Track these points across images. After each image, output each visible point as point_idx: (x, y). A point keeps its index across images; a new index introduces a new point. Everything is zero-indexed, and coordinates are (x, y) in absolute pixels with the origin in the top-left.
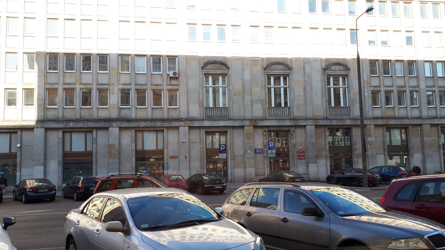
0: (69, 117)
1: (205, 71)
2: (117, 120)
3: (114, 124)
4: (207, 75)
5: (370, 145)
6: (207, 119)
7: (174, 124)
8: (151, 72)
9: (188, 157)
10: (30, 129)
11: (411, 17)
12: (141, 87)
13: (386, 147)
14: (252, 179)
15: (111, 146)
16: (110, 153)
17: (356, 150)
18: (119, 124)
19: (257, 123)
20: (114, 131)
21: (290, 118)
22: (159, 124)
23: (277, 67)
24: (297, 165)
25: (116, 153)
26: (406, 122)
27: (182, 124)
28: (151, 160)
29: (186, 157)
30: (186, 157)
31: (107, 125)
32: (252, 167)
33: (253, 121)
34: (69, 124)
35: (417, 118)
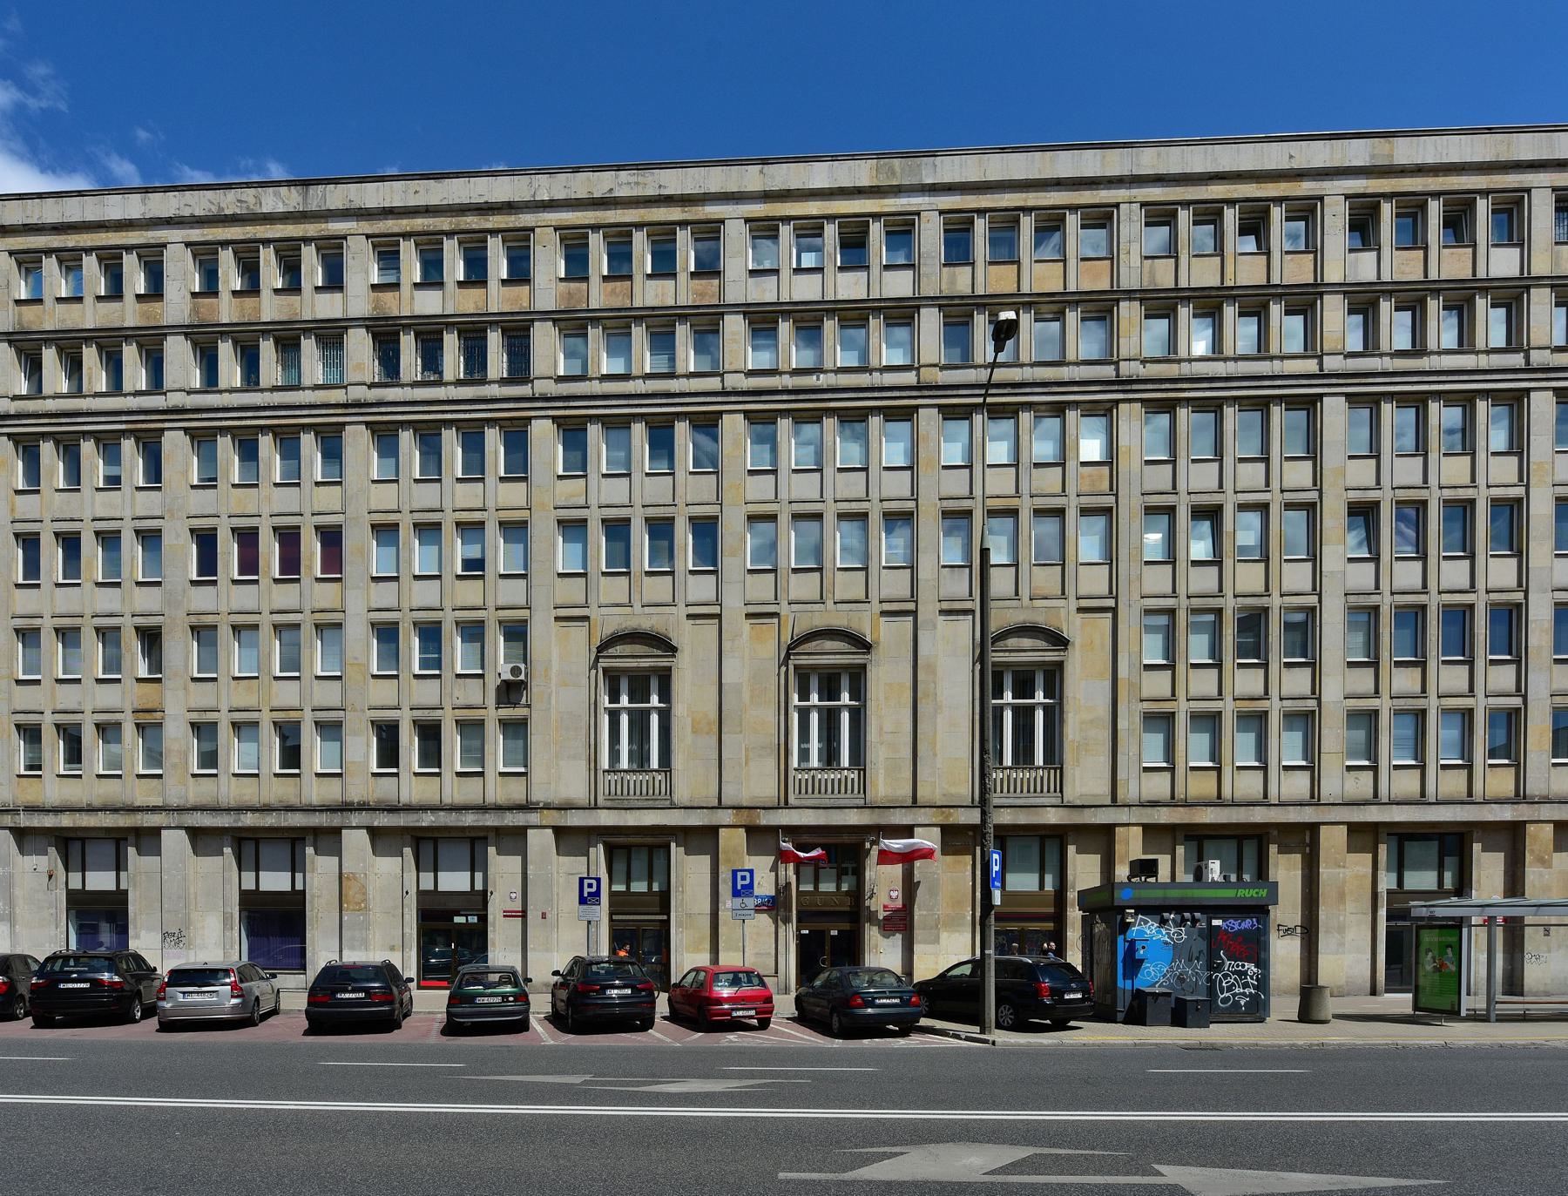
0: (246, 798)
1: (603, 663)
3: (355, 819)
6: (609, 804)
22: (469, 819)
23: (829, 645)
26: (1259, 816)
27: (534, 818)
31: (335, 820)
33: (746, 812)
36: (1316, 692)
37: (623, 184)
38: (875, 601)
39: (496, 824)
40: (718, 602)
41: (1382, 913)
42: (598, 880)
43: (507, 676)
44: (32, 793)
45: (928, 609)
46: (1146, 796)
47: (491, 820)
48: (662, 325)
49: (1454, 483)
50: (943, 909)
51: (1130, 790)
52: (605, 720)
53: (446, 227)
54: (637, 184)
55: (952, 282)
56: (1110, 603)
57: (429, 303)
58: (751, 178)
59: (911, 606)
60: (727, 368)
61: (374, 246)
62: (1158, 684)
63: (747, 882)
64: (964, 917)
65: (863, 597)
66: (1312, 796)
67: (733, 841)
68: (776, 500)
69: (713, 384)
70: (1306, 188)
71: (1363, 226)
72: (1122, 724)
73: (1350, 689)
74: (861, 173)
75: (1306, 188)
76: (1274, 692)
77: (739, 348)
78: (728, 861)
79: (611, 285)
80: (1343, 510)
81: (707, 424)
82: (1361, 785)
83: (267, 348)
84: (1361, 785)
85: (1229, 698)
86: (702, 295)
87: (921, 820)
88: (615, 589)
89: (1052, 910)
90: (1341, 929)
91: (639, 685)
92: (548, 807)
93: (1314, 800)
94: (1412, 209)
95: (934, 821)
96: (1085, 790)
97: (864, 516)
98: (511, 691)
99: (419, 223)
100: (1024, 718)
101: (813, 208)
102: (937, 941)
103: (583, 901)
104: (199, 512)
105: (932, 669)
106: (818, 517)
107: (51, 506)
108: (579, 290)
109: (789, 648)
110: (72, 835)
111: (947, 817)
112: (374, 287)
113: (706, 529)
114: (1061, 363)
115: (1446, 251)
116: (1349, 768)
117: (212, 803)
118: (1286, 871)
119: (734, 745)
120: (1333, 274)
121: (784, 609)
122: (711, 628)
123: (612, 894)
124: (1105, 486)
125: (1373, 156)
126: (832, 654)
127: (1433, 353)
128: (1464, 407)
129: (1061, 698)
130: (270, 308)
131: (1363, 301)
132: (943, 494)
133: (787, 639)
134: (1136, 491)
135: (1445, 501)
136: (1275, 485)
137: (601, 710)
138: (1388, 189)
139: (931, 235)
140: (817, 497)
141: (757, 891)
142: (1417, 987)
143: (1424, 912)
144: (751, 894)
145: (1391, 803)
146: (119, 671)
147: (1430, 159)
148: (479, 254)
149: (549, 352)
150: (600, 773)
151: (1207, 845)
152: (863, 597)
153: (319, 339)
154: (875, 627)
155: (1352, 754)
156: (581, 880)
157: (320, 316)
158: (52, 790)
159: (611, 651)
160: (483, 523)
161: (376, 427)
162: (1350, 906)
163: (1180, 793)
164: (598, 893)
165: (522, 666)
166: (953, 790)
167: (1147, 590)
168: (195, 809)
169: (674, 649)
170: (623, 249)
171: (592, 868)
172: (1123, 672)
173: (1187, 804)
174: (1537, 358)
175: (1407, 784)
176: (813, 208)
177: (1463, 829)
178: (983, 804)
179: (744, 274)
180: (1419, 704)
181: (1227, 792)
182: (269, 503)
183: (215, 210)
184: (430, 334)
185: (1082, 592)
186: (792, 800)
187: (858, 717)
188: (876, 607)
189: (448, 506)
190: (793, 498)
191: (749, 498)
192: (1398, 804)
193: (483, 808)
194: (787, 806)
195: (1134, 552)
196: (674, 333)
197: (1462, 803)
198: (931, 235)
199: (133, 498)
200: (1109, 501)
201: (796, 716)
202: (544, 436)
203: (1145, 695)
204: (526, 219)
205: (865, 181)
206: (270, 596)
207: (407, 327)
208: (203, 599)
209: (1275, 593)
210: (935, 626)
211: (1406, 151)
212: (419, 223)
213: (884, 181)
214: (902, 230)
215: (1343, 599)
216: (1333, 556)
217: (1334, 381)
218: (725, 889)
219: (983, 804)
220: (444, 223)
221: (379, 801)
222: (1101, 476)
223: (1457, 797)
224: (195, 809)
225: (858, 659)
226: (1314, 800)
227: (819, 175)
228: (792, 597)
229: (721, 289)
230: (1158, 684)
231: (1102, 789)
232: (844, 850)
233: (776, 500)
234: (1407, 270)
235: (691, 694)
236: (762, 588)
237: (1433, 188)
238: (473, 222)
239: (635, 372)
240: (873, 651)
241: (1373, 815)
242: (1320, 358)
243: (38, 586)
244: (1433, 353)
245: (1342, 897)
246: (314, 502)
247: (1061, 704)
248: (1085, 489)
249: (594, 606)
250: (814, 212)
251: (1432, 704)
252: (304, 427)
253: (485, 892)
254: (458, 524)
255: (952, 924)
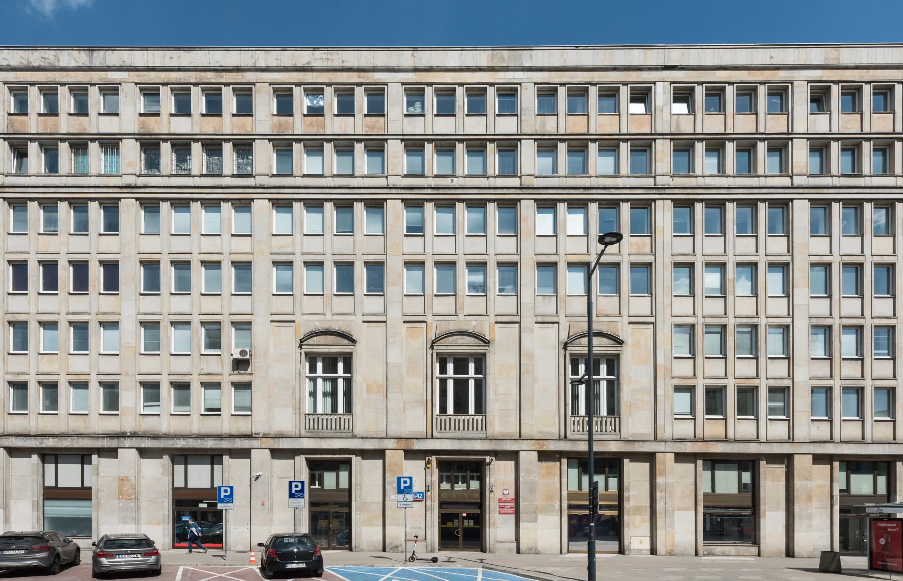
0: (49, 429)
1: (306, 348)
2: (134, 435)
3: (128, 442)
4: (312, 358)
5: (661, 492)
6: (309, 435)
7: (239, 444)
8: (199, 350)
9: (267, 504)
10: (679, 509)
11: (653, 174)
12: (179, 377)
13: (700, 497)
14: (397, 547)
15: (123, 480)
16: (121, 492)
17: (628, 500)
18: (136, 442)
19: (413, 444)
20: (128, 455)
21: (484, 436)
22: (210, 444)
23: (460, 339)
24: (494, 524)
25: (131, 491)
26: (753, 448)
27: (256, 443)
28: (201, 505)
29: (263, 504)
30: (263, 504)
31: (113, 443)
32: (398, 525)
33: (404, 441)
34: (45, 441)
35: (496, 391)
36: (790, 375)
37: (318, 58)
38: (492, 316)
39: (229, 446)
40: (385, 313)
41: (837, 508)
42: (302, 483)
43: (237, 356)
44: (16, 424)
45: (528, 320)
46: (676, 436)
47: (225, 444)
48: (345, 146)
49: (881, 253)
50: (539, 502)
51: (665, 431)
52: (437, 382)
53: (193, 80)
54: (327, 59)
55: (543, 125)
56: (652, 319)
57: (182, 126)
58: (406, 58)
59: (517, 319)
60: (390, 172)
61: (274, 91)
62: (685, 368)
63: (408, 484)
64: (554, 506)
65: (484, 313)
66: (789, 438)
67: (395, 457)
68: (557, 254)
69: (382, 182)
70: (782, 75)
71: (819, 98)
72: (660, 392)
73: (813, 374)
74: (482, 57)
75: (782, 75)
76: (762, 374)
77: (397, 157)
78: (392, 471)
79: (368, 119)
80: (807, 266)
81: (376, 206)
82: (822, 431)
83: (64, 149)
84: (822, 431)
85: (731, 378)
86: (372, 128)
87: (524, 447)
88: (445, 305)
89: (616, 503)
90: (809, 517)
91: (330, 363)
92: (266, 436)
93: (790, 439)
94: (852, 92)
95: (533, 448)
96: (635, 431)
97: (555, 265)
98: (240, 364)
99: (174, 76)
100: (462, 387)
101: (449, 78)
102: (535, 520)
103: (292, 495)
104: (14, 250)
105: (531, 357)
106: (555, 265)
107: (34, 246)
108: (287, 122)
109: (433, 342)
110: (47, 452)
111: (542, 446)
112: (141, 115)
113: (376, 269)
114: (352, 176)
115: (875, 116)
116: (812, 421)
117: (218, 432)
118: (772, 480)
119: (282, 401)
120: (799, 127)
121: (429, 318)
122: (379, 329)
123: (310, 490)
124: (648, 250)
125: (826, 59)
126: (463, 346)
127: (866, 176)
128: (887, 209)
129: (618, 376)
130: (65, 124)
131: (414, 145)
132: (538, 252)
133: (564, 337)
134: (668, 253)
135: (875, 264)
136: (761, 251)
137: (303, 377)
138: (836, 78)
139: (528, 98)
140: (453, 252)
141: (415, 489)
142: (871, 553)
143: (875, 510)
144: (411, 492)
145: (842, 442)
146: (26, 349)
147: (865, 61)
148: (216, 98)
149: (529, 158)
150: (303, 416)
151: (717, 465)
152: (484, 313)
153: (72, 146)
154: (492, 330)
155: (878, 413)
156: (291, 483)
157: (101, 132)
158: (165, 425)
159: (310, 341)
160: (220, 262)
161: (144, 201)
162: (815, 504)
163: (699, 434)
164: (302, 491)
165: (248, 350)
166: (546, 430)
167: (675, 312)
168: (11, 435)
169: (354, 341)
170: (216, 98)
171: (297, 474)
172: (660, 361)
173: (704, 440)
174: (798, 181)
175: (854, 431)
176: (449, 78)
177: (890, 459)
178: (591, 440)
179: (401, 116)
180: (860, 384)
181: (731, 434)
182: (65, 246)
183: (25, 63)
184: (182, 147)
185: (631, 313)
186: (436, 434)
187: (480, 386)
188: (492, 318)
189: (298, 251)
190: (436, 252)
191: (405, 251)
192: (847, 442)
193: (220, 437)
194: (432, 437)
195: (667, 290)
196: (292, 150)
197: (889, 443)
198: (528, 98)
199: (332, 242)
200: (650, 259)
201: (438, 381)
202: (801, 212)
203: (675, 374)
204: (250, 77)
205: (484, 63)
206: (64, 304)
207: (165, 140)
208: (150, 304)
209: (762, 316)
210: (532, 331)
211: (848, 55)
212: (174, 76)
213: (497, 63)
214: (509, 94)
215: (807, 321)
216: (801, 293)
217: (801, 191)
218: (392, 487)
219: (591, 440)
220: (192, 77)
221: (145, 432)
222: (644, 244)
223: (885, 439)
224: (11, 435)
225: (481, 350)
226: (790, 439)
227: (453, 58)
228: (435, 311)
229: (386, 125)
230: (685, 368)
231: (648, 431)
232: (463, 466)
233: (557, 254)
234: (849, 126)
235: (366, 370)
236: (415, 306)
237: (866, 78)
238: (210, 77)
239: (326, 174)
240: (491, 345)
241: (829, 449)
242: (791, 177)
243: (26, 294)
244: (866, 176)
245: (809, 498)
246: (96, 246)
247: (485, 378)
248: (634, 251)
249: (298, 315)
250: (449, 81)
251: (868, 385)
252: (490, 200)
253: (350, 490)
254: (305, 263)
255: (546, 510)
